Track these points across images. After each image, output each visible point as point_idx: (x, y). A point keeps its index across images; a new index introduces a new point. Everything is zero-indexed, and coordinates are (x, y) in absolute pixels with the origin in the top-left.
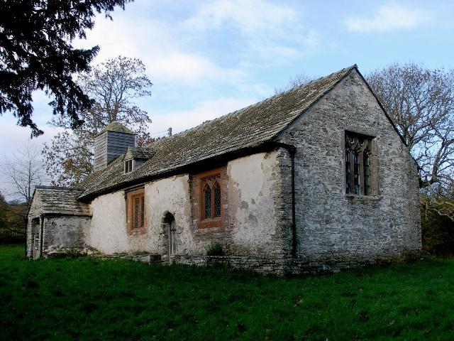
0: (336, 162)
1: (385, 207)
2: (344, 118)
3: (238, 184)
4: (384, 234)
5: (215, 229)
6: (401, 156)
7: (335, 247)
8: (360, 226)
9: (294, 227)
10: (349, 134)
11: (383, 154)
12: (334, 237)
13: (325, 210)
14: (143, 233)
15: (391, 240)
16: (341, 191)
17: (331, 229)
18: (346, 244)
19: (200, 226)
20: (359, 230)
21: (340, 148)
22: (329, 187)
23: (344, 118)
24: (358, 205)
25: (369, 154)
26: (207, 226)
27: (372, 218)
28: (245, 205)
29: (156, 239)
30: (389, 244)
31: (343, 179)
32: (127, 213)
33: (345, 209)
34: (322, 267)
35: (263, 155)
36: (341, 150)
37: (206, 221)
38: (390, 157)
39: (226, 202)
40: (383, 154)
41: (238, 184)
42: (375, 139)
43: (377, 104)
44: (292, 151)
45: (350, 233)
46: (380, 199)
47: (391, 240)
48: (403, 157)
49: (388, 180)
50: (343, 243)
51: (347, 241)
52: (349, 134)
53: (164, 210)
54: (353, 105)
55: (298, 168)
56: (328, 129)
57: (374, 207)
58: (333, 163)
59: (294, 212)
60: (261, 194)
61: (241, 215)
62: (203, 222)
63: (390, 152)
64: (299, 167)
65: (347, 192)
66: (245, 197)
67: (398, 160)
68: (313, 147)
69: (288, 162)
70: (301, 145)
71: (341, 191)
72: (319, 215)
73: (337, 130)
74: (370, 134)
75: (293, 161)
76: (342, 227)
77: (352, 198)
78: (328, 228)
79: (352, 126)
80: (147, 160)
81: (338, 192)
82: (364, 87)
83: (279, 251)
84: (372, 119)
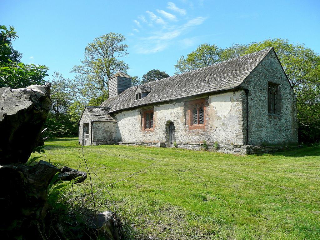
0: (264, 97)
1: (283, 121)
2: (268, 75)
3: (215, 108)
4: (283, 134)
5: (200, 130)
6: (290, 94)
7: (263, 140)
8: (273, 130)
9: (247, 130)
10: (270, 84)
11: (283, 93)
12: (263, 135)
13: (260, 121)
14: (152, 131)
15: (285, 137)
16: (266, 112)
17: (261, 131)
18: (267, 139)
19: (190, 129)
20: (273, 132)
21: (266, 90)
22: (261, 110)
23: (268, 75)
24: (272, 119)
25: (133, 85)
26: (195, 128)
27: (278, 126)
28: (219, 118)
29: (162, 134)
30: (285, 139)
31: (267, 106)
32: (142, 121)
33: (267, 121)
34: (262, 150)
35: (232, 93)
36: (265, 92)
37: (194, 125)
38: (286, 95)
39: (208, 116)
40: (283, 93)
41: (215, 108)
42: (280, 86)
43: (281, 68)
44: (247, 92)
45: (269, 133)
46: (281, 116)
47: (285, 137)
48: (291, 95)
49: (285, 107)
50: (266, 138)
51: (268, 137)
52: (270, 84)
53: (167, 120)
54: (271, 68)
55: (249, 101)
56: (261, 81)
57: (279, 120)
58: (262, 98)
59: (247, 123)
60: (229, 113)
61: (217, 123)
62: (192, 126)
63: (286, 92)
64: (250, 100)
65: (268, 113)
66: (220, 114)
67: (289, 96)
68: (255, 90)
69: (245, 97)
70: (250, 89)
71: (266, 112)
72: (257, 124)
73: (265, 81)
74: (278, 83)
75: (247, 97)
76: (266, 130)
77: (270, 115)
78: (260, 131)
79: (270, 79)
80: (149, 93)
81: (265, 112)
82: (276, 59)
83: (240, 142)
84: (279, 76)
